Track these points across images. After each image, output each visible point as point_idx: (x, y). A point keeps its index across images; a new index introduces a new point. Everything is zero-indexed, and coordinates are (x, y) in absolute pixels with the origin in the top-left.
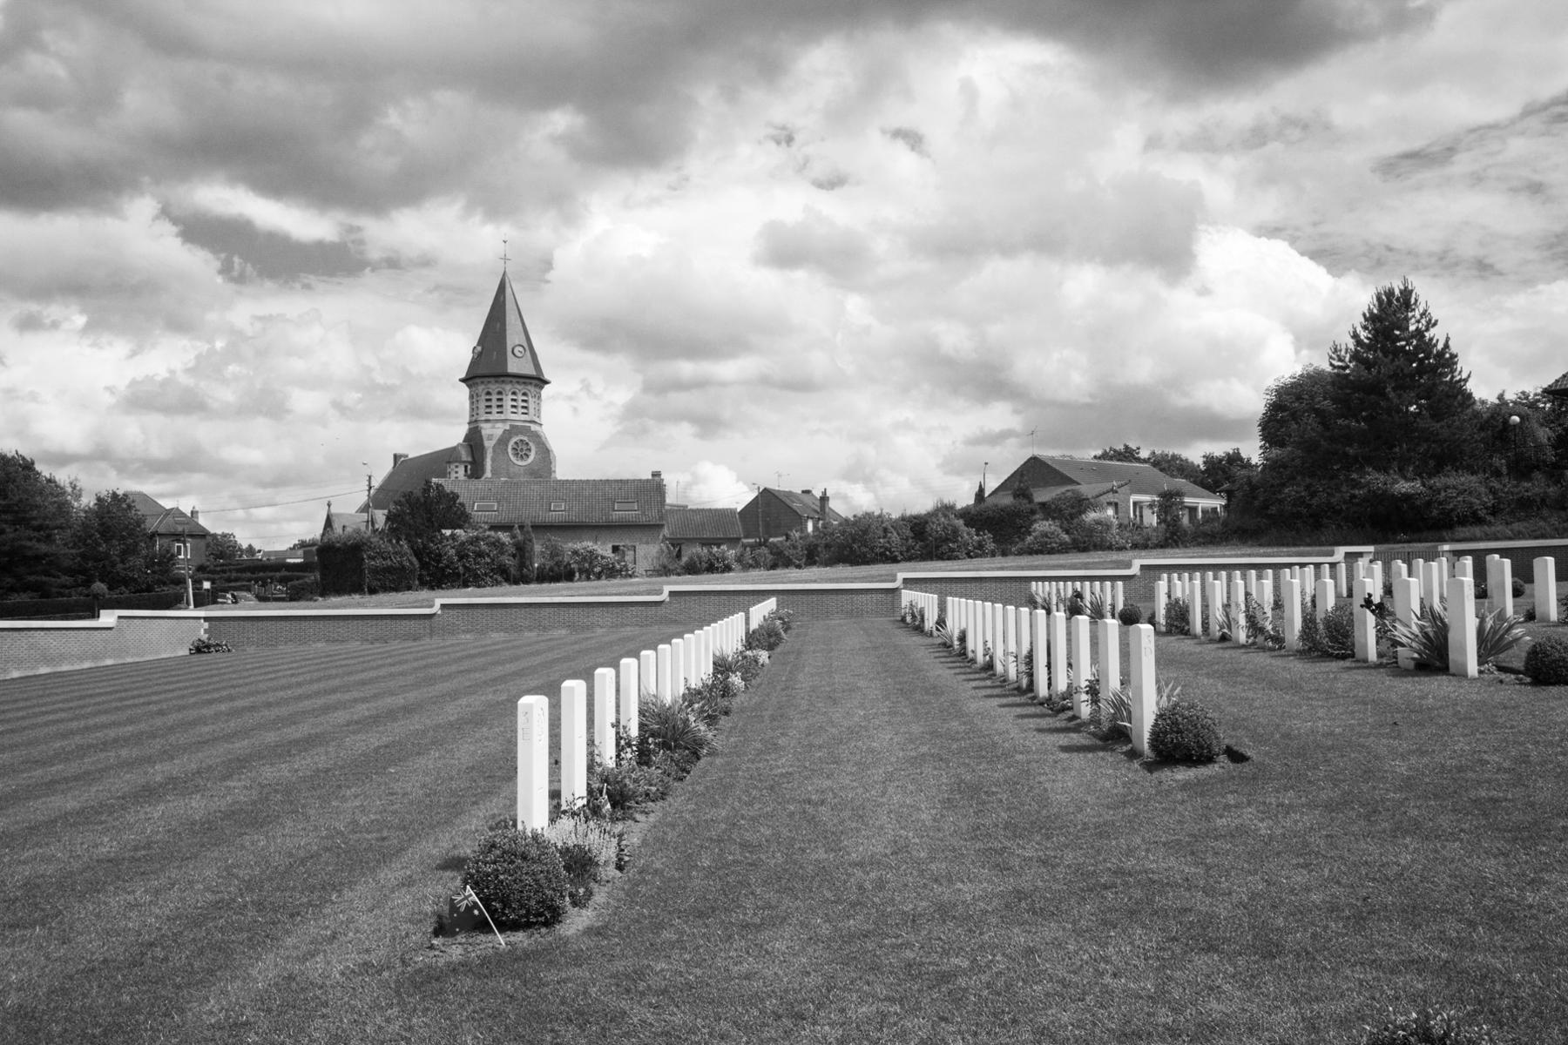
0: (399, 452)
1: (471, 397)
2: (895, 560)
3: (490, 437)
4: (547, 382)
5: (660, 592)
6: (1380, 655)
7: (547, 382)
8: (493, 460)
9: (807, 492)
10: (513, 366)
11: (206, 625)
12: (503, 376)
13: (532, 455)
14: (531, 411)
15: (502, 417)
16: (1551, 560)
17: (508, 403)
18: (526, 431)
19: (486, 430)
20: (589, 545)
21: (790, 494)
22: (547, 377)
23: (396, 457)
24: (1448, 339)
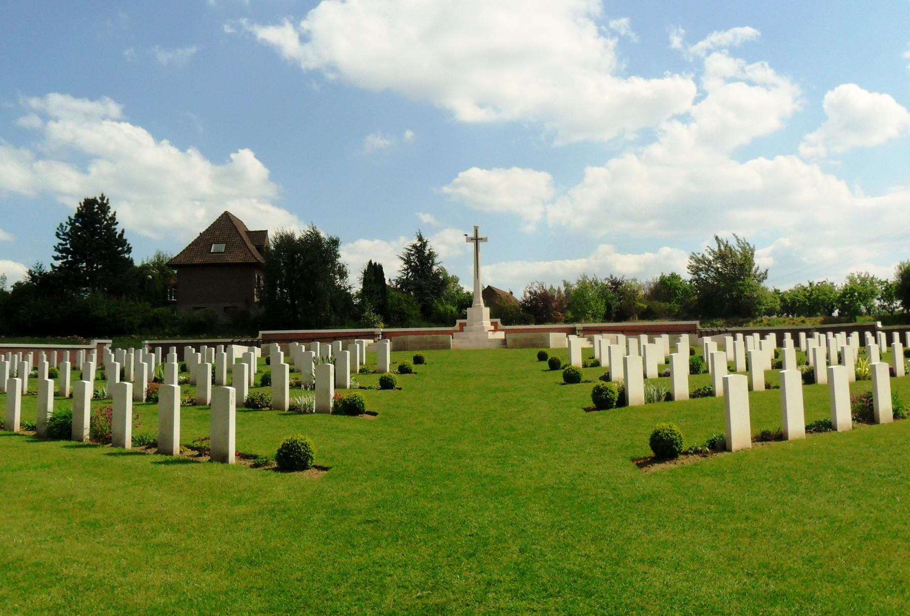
24: (123, 231)
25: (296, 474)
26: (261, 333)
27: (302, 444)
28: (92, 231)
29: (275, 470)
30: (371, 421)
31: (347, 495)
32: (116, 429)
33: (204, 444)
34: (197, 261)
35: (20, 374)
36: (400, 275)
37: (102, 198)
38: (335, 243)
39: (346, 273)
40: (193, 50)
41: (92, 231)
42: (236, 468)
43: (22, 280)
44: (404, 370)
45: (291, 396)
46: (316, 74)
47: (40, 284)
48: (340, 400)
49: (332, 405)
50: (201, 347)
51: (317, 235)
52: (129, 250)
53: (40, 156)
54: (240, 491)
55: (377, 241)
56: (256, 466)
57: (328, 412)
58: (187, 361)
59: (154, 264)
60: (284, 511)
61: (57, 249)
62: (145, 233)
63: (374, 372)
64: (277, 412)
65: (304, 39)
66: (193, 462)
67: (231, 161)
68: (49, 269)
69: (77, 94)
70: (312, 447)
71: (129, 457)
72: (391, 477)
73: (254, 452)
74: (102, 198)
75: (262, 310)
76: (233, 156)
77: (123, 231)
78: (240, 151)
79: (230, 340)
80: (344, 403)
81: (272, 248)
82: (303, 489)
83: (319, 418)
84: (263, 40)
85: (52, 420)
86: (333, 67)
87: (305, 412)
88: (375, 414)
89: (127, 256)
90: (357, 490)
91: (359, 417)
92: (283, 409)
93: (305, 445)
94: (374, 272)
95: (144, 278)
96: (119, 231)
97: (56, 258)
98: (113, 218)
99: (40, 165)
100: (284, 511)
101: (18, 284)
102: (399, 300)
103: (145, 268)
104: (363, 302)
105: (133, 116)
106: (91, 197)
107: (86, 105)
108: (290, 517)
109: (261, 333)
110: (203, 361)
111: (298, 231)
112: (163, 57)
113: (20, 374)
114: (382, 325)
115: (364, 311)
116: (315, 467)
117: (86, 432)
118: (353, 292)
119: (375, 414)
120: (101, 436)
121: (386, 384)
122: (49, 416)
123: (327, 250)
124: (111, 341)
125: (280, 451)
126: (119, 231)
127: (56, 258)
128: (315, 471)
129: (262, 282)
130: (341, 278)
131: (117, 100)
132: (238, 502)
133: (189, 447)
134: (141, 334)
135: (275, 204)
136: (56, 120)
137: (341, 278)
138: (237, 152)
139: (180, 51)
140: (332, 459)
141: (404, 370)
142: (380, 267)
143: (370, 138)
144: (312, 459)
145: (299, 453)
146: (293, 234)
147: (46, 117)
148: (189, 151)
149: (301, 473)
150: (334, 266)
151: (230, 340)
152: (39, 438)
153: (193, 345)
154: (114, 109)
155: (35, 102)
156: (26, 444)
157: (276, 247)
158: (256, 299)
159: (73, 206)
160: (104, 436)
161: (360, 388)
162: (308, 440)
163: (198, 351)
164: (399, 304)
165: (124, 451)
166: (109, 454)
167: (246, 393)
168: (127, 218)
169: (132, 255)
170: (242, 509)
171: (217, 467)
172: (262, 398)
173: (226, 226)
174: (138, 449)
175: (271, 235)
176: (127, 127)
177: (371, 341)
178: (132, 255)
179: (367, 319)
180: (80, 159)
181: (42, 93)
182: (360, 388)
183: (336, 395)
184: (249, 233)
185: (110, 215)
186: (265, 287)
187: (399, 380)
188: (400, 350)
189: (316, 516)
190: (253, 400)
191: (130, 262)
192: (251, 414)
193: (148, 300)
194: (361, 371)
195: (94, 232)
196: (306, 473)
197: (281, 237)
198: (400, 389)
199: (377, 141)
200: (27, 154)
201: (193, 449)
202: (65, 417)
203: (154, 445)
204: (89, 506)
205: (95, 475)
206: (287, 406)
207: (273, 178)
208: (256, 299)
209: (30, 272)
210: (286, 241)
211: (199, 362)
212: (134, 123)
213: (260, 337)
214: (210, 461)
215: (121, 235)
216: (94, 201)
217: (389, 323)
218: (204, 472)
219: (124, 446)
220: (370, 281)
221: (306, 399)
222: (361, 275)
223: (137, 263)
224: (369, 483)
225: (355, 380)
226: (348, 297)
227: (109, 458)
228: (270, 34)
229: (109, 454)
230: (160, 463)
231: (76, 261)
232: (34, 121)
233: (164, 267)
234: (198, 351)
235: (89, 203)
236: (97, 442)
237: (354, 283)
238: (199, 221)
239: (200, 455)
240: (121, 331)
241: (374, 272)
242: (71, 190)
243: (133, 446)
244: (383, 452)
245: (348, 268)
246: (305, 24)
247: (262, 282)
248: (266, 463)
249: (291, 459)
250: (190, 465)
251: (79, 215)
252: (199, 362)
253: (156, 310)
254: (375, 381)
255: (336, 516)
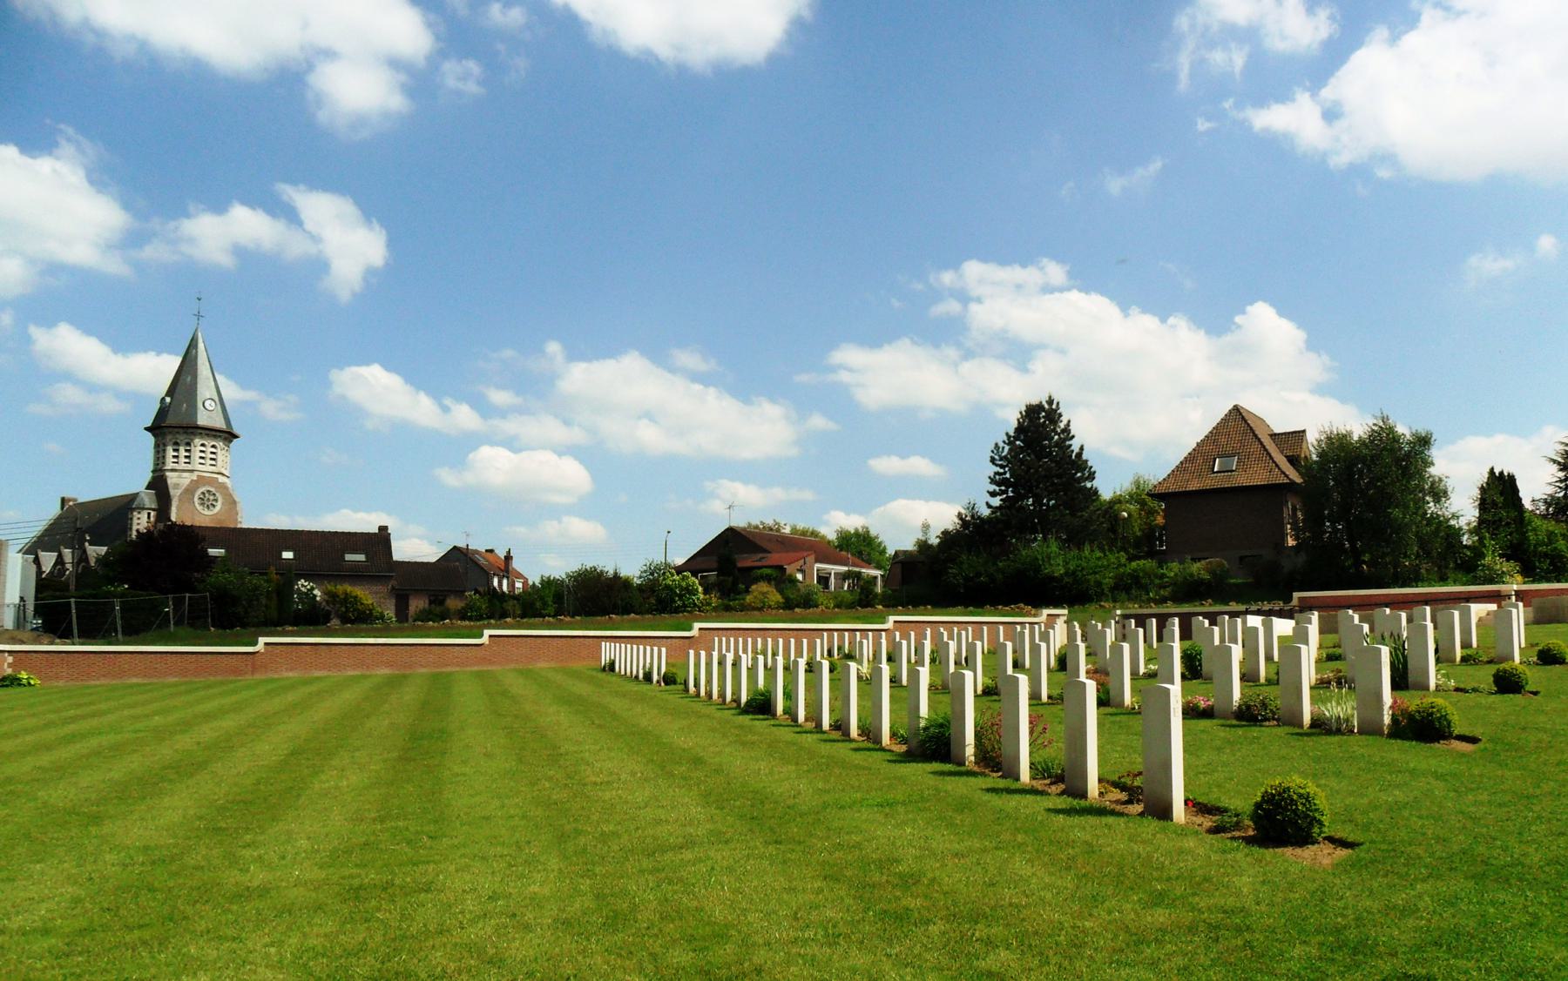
0: (67, 495)
1: (157, 446)
2: (480, 618)
3: (177, 486)
4: (236, 437)
5: (690, 629)
6: (1049, 697)
7: (236, 437)
8: (178, 508)
9: (491, 551)
10: (203, 420)
11: (10, 659)
12: (193, 430)
13: (219, 506)
14: (219, 462)
15: (189, 467)
16: (1176, 620)
17: (196, 454)
18: (212, 482)
19: (172, 478)
20: (349, 588)
21: (476, 552)
22: (236, 430)
23: (63, 501)
24: (1082, 448)
25: (1288, 851)
26: (1296, 595)
27: (1301, 796)
28: (1038, 452)
29: (1249, 841)
30: (1464, 755)
31: (1376, 906)
32: (1006, 750)
33: (1138, 782)
34: (1194, 486)
35: (969, 662)
36: (1550, 490)
37: (1050, 402)
38: (1424, 441)
39: (1445, 492)
40: (1156, 165)
41: (1038, 452)
42: (1182, 831)
43: (951, 528)
44: (1548, 657)
45: (1313, 700)
46: (1359, 171)
47: (973, 534)
48: (1405, 712)
49: (1387, 720)
50: (1219, 618)
51: (1391, 430)
52: (1092, 477)
53: (968, 355)
54: (1169, 879)
55: (1500, 438)
56: (1215, 830)
57: (1381, 733)
58: (1198, 640)
59: (1131, 496)
60: (1239, 930)
61: (993, 481)
62: (1117, 451)
63: (1490, 662)
64: (1282, 731)
65: (1331, 115)
66: (1113, 813)
67: (1239, 327)
68: (986, 512)
69: (1003, 258)
70: (1321, 802)
71: (1017, 797)
72: (1479, 878)
73: (1225, 802)
74: (1050, 402)
75: (1301, 559)
76: (1238, 319)
77: (1082, 448)
78: (1249, 308)
79: (1242, 608)
80: (1411, 717)
81: (1314, 457)
82: (1291, 887)
83: (1359, 745)
84: (1266, 130)
85: (926, 729)
86: (1388, 158)
87: (1338, 732)
88: (1473, 740)
89: (1089, 485)
90: (1399, 899)
91: (1440, 746)
92: (1301, 726)
93: (1307, 797)
94: (1500, 490)
95: (1116, 518)
96: (1076, 448)
97: (993, 494)
98: (1066, 430)
99: (967, 367)
100: (1239, 930)
101: (945, 533)
102: (1550, 534)
103: (1117, 501)
104: (1481, 540)
105: (1085, 279)
106: (1035, 401)
107: (1016, 273)
108: (1248, 944)
109: (1296, 595)
110: (1222, 640)
111: (1357, 427)
112: (1115, 185)
113: (969, 662)
114: (1519, 578)
115: (1483, 556)
116: (1331, 840)
117: (970, 751)
118: (1462, 523)
119: (1473, 740)
120: (992, 759)
121: (1508, 683)
122: (923, 724)
123: (1408, 455)
124: (1065, 612)
125: (1258, 806)
126: (1076, 448)
127: (993, 494)
128: (1327, 848)
129: (1299, 514)
130: (1437, 500)
131: (1058, 258)
132: (1158, 900)
133: (1115, 785)
134: (1115, 601)
135: (1320, 390)
136: (979, 300)
137: (1437, 500)
138: (1244, 313)
139: (1140, 171)
140: (1366, 827)
141: (1548, 657)
142: (1512, 479)
143: (1473, 260)
144: (1321, 824)
145: (1295, 812)
146: (1350, 434)
147: (964, 298)
148: (1171, 320)
149: (1298, 851)
150: (1422, 478)
151: (1242, 608)
152: (909, 757)
153: (1206, 615)
154: (1055, 272)
155: (947, 277)
156: (885, 764)
157: (1320, 455)
158: (1291, 542)
159: (1011, 419)
160: (994, 759)
161: (1457, 690)
162: (1311, 788)
163: (1213, 623)
164: (1550, 542)
165: (1015, 786)
166: (988, 790)
167: (924, 711)
168: (1089, 431)
169: (1096, 483)
170: (1160, 916)
171: (1152, 825)
172: (1264, 705)
173: (1237, 425)
174: (1038, 784)
175: (1312, 437)
176: (1075, 296)
177: (1493, 607)
178: (1096, 483)
179: (1489, 568)
180: (1018, 352)
181: (955, 264)
182: (1457, 690)
183: (1395, 702)
184: (1274, 436)
185: (1062, 425)
186: (1326, 520)
187: (1534, 677)
188: (1550, 622)
189: (1297, 951)
190: (1248, 707)
191: (1094, 493)
192: (1240, 731)
193: (1124, 549)
194: (1464, 659)
195: (1041, 453)
196: (1308, 852)
197: (1329, 438)
198: (1535, 693)
199: (1487, 265)
200: (951, 352)
201: (1123, 788)
202: (941, 726)
203: (1059, 779)
204: (909, 881)
205: (951, 825)
206: (1307, 719)
207: (1312, 345)
208: (1291, 542)
209: (960, 516)
210: (1339, 449)
211: (1217, 642)
212: (1085, 289)
213: (1295, 602)
214: (1142, 814)
215: (1079, 455)
216: (1040, 407)
217: (1529, 572)
218: (1125, 836)
219: (1017, 779)
220: (1494, 504)
221: (1341, 708)
222: (1476, 493)
223: (1106, 494)
224: (1427, 886)
225: (1447, 676)
226: (1455, 533)
227: (987, 797)
228: (1274, 118)
229: (988, 790)
230: (1058, 811)
231: (1019, 497)
232: (953, 306)
233: (1146, 497)
234: (1213, 623)
235: (1032, 411)
236: (987, 766)
237: (1462, 508)
238: (1188, 427)
239: (1130, 802)
240: (1072, 594)
241: (1500, 490)
242: (1009, 399)
243: (1033, 778)
244: (1475, 820)
245: (1450, 484)
246: (1327, 93)
247: (1299, 514)
248: (1237, 826)
249: (1280, 823)
250: (1110, 820)
251: (1020, 429)
252: (1217, 642)
253: (1134, 564)
254: (1484, 676)
255: (1338, 956)
